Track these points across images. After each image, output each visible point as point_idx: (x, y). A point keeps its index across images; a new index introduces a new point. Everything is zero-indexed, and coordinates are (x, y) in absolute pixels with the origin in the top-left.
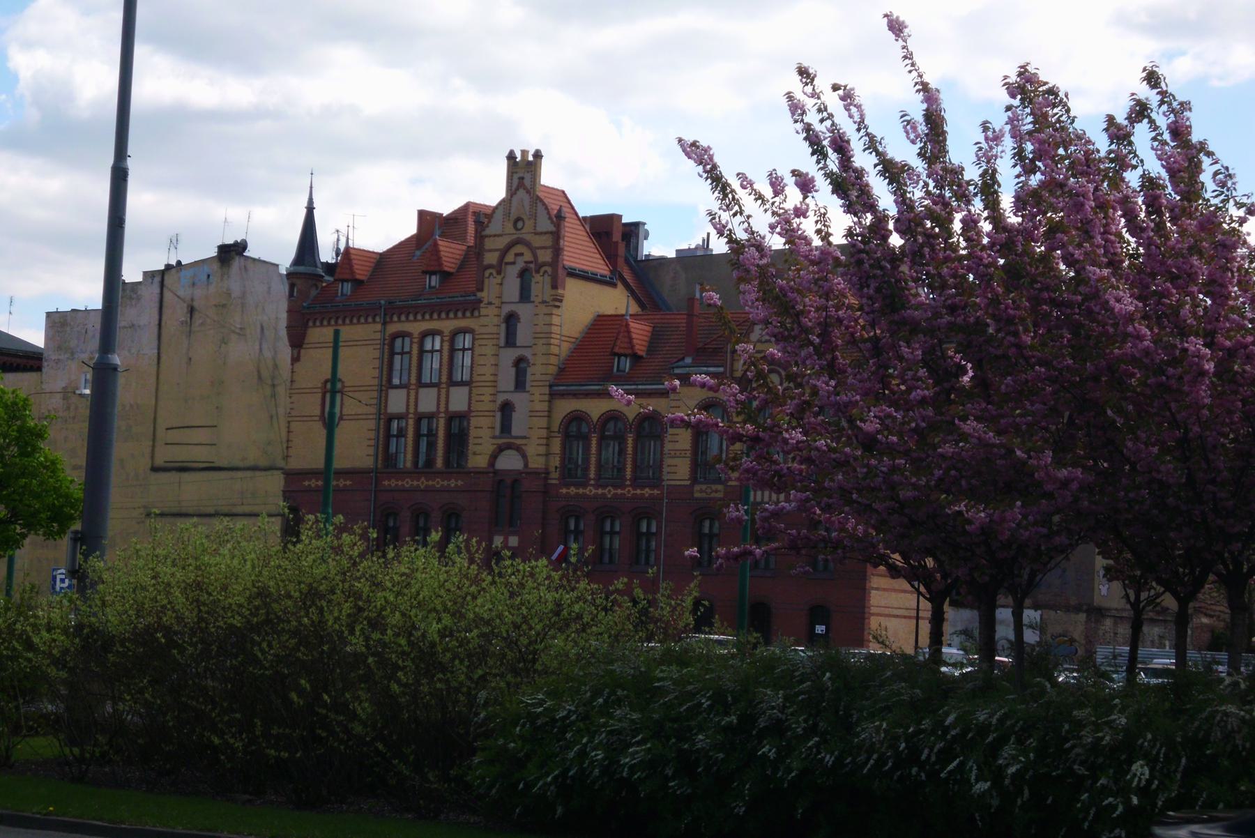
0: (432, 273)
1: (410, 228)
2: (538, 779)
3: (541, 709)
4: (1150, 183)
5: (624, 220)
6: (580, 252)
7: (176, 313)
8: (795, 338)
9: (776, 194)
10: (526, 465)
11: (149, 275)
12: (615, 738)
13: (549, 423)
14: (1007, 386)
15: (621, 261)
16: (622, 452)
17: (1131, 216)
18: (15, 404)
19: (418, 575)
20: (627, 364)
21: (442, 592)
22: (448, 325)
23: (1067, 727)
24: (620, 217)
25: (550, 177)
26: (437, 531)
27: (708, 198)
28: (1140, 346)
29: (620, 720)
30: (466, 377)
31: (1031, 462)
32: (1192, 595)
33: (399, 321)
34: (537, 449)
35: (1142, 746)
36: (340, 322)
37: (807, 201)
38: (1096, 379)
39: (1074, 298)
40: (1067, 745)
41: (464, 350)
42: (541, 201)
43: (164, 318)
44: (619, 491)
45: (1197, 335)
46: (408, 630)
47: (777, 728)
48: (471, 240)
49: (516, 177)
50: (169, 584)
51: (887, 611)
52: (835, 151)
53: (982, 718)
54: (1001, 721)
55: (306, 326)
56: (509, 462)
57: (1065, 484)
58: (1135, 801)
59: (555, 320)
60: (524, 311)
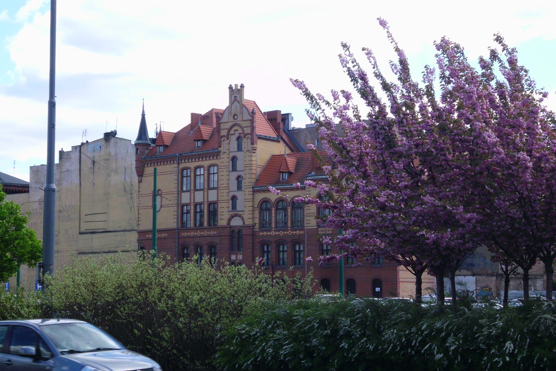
0: (198, 140)
1: (188, 121)
2: (245, 362)
3: (244, 331)
4: (500, 86)
5: (282, 113)
6: (263, 128)
7: (87, 164)
8: (348, 162)
9: (335, 99)
10: (244, 223)
11: (74, 148)
12: (277, 343)
13: (253, 204)
14: (442, 178)
15: (281, 131)
16: (286, 215)
17: (492, 101)
18: (12, 208)
19: (188, 275)
20: (286, 176)
21: (199, 281)
22: (206, 163)
23: (476, 328)
24: (280, 111)
25: (248, 96)
26: (196, 255)
27: (306, 104)
28: (499, 157)
29: (279, 335)
30: (215, 186)
31: (453, 211)
32: (529, 267)
33: (185, 162)
34: (248, 215)
35: (509, 334)
36: (156, 164)
37: (349, 103)
38: (481, 173)
39: (470, 138)
40: (476, 336)
41: (214, 174)
42: (245, 106)
43: (82, 166)
44: (286, 233)
45: (523, 151)
46: (185, 299)
47: (348, 335)
48: (215, 125)
49: (233, 96)
50: (79, 285)
51: (407, 280)
52: (361, 79)
53: (438, 326)
54: (447, 327)
55: (144, 167)
56: (236, 222)
57: (469, 220)
58: (508, 359)
59: (254, 158)
60: (239, 155)
